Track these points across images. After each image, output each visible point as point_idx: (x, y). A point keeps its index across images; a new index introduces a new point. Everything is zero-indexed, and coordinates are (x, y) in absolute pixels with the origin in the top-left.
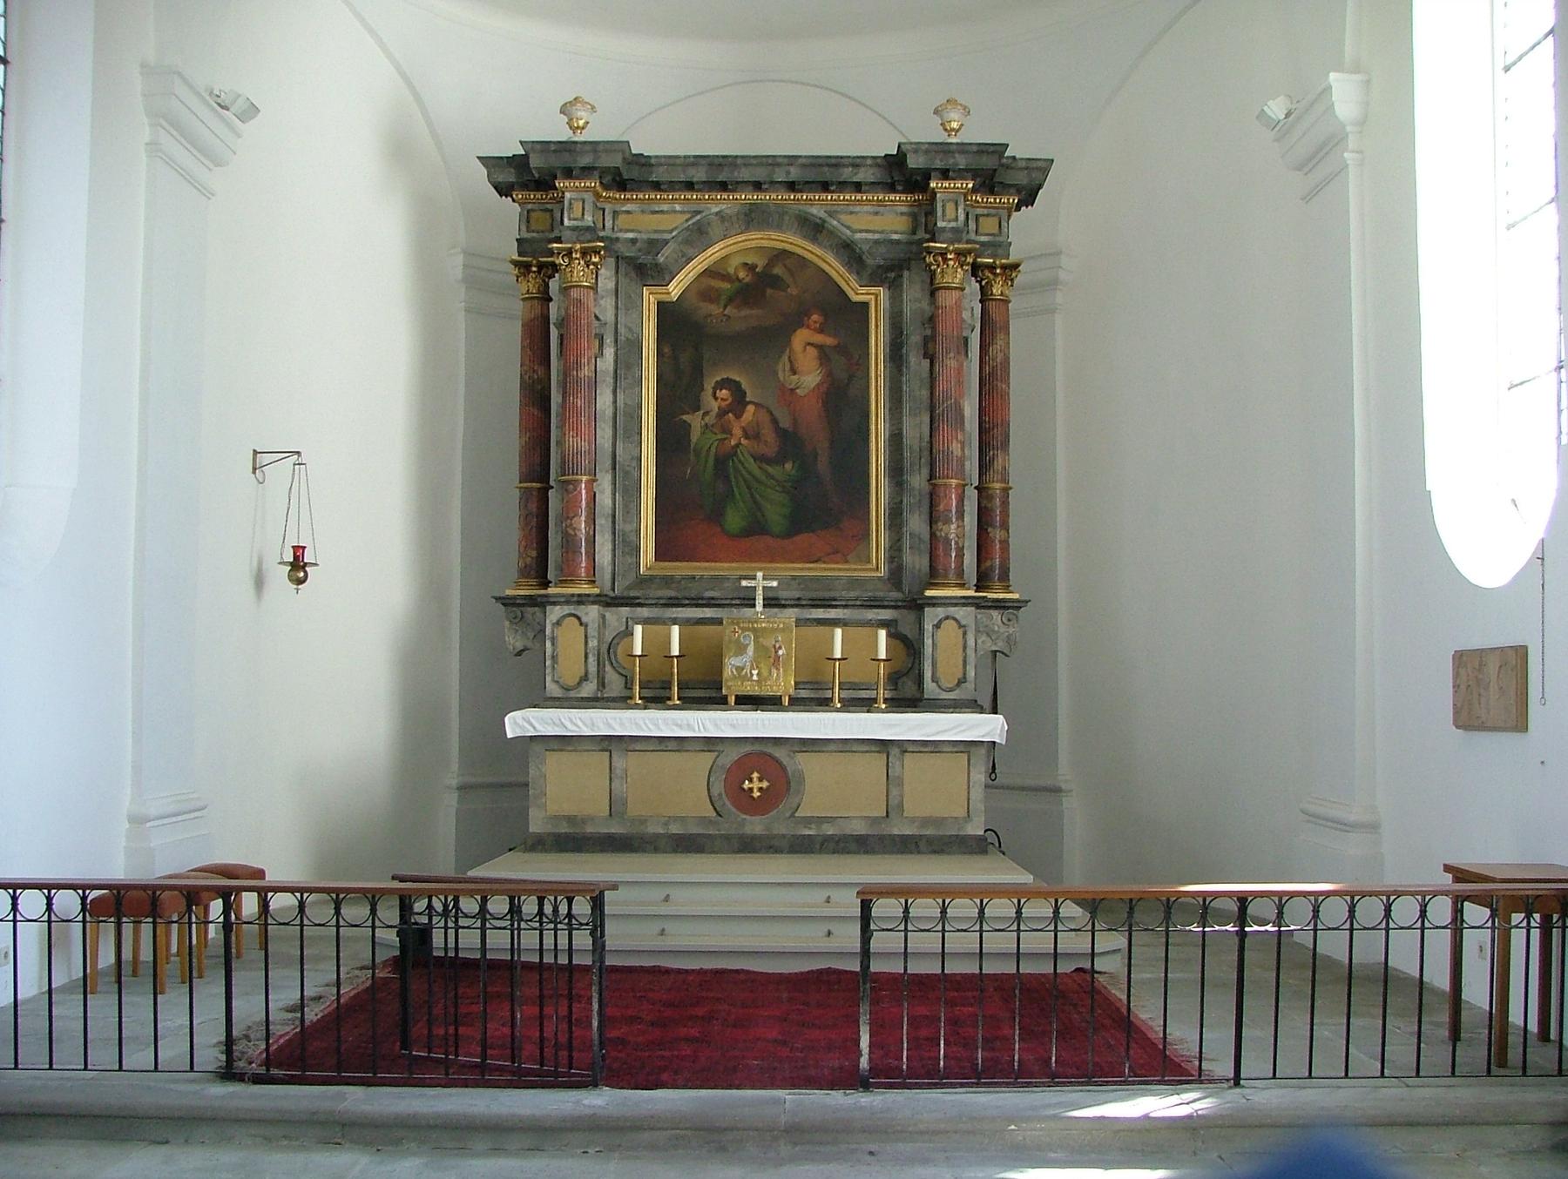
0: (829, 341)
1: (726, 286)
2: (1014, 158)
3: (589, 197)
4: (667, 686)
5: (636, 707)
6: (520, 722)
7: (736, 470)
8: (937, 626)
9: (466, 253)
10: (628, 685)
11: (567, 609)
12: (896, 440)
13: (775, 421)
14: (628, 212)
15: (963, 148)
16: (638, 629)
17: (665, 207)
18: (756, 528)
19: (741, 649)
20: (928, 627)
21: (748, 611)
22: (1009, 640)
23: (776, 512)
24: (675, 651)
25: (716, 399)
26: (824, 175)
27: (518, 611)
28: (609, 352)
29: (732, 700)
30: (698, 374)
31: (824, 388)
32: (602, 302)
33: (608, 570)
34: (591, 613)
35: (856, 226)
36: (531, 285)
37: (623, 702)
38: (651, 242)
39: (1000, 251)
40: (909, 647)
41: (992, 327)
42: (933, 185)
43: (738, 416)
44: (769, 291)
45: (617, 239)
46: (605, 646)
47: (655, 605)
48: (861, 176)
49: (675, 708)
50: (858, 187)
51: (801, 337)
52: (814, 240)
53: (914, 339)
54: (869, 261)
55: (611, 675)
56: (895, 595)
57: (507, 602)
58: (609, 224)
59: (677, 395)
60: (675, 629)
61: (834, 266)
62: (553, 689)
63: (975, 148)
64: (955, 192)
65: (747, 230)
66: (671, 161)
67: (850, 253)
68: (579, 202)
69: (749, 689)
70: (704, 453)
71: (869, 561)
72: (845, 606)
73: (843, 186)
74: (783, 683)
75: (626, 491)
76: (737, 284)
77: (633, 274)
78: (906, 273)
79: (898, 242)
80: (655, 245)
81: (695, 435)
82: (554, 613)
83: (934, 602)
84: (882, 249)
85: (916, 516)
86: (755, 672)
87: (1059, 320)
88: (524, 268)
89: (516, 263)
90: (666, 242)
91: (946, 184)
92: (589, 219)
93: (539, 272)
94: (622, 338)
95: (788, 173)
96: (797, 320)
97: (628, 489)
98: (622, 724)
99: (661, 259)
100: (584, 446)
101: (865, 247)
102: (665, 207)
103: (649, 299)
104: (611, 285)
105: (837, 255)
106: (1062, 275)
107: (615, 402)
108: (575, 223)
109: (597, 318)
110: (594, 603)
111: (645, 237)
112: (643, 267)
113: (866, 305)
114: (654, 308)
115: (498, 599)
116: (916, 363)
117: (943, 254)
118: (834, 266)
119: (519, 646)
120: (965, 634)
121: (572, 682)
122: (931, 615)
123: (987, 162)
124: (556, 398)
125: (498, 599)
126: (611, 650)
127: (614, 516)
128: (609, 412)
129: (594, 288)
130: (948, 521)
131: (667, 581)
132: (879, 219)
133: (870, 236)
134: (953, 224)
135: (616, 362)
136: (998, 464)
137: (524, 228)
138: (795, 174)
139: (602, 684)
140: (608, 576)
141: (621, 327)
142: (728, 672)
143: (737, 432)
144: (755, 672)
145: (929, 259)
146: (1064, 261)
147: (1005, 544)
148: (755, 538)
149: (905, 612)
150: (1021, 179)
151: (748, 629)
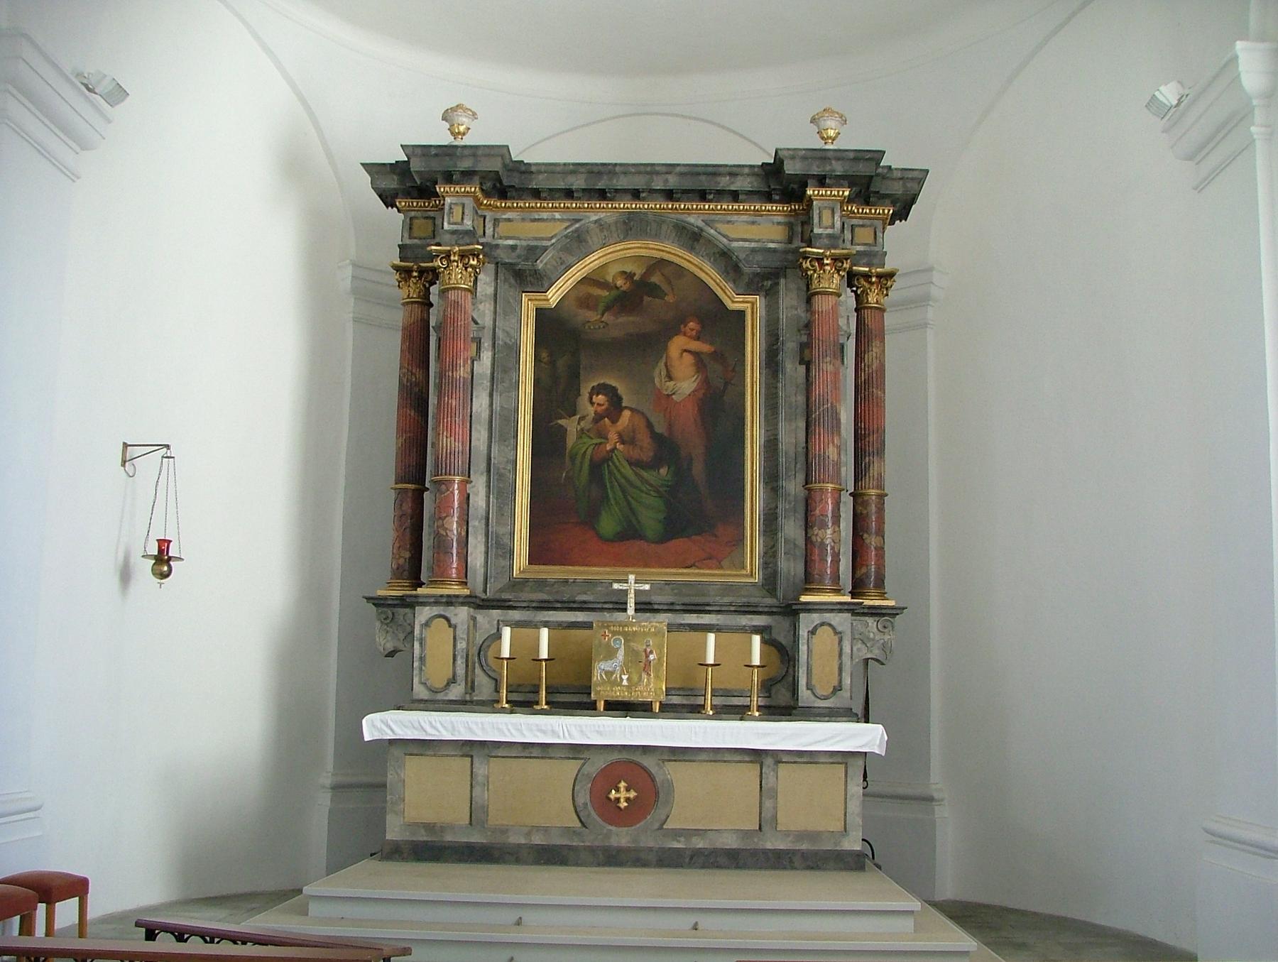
3: (469, 202)
5: (503, 711)
6: (379, 724)
8: (813, 632)
10: (497, 690)
11: (436, 610)
12: (771, 446)
13: (650, 425)
14: (509, 220)
15: (840, 155)
16: (507, 632)
17: (545, 215)
18: (630, 532)
19: (611, 654)
20: (803, 633)
21: (619, 616)
23: (650, 517)
24: (544, 654)
25: (592, 403)
26: (702, 185)
28: (487, 356)
29: (601, 705)
31: (700, 394)
32: (481, 307)
33: (481, 572)
34: (461, 614)
36: (412, 290)
37: (490, 706)
38: (531, 249)
39: (875, 261)
40: (783, 654)
41: (867, 335)
42: (809, 192)
44: (647, 299)
45: (497, 246)
46: (474, 651)
48: (741, 184)
50: (735, 196)
51: (677, 344)
52: (691, 249)
53: (790, 345)
54: (746, 270)
55: (481, 678)
56: (769, 601)
57: (378, 602)
58: (489, 231)
60: (544, 633)
61: (711, 275)
62: (420, 692)
63: (851, 155)
66: (551, 169)
67: (728, 262)
68: (459, 206)
69: (619, 694)
70: (578, 462)
71: (743, 568)
72: (719, 612)
73: (721, 194)
74: (652, 689)
75: (500, 494)
76: (614, 293)
77: (512, 281)
78: (782, 281)
79: (774, 250)
80: (534, 252)
81: (571, 439)
82: (423, 614)
83: (810, 608)
84: (759, 258)
86: (625, 677)
87: (929, 331)
88: (405, 273)
90: (545, 249)
92: (468, 224)
93: (420, 277)
95: (667, 181)
96: (672, 328)
97: (502, 491)
99: (540, 265)
101: (742, 256)
102: (545, 215)
103: (528, 306)
104: (490, 290)
105: (714, 264)
106: (934, 291)
108: (455, 227)
110: (463, 604)
111: (524, 243)
112: (523, 274)
113: (741, 313)
114: (532, 314)
115: (369, 599)
116: (792, 370)
118: (711, 275)
119: (390, 646)
120: (841, 641)
122: (806, 622)
123: (863, 169)
124: (433, 400)
125: (369, 599)
127: (487, 519)
129: (473, 291)
130: (823, 526)
131: (541, 584)
132: (756, 228)
133: (746, 244)
134: (829, 231)
136: (874, 471)
137: (406, 235)
138: (673, 182)
139: (471, 687)
140: (480, 579)
143: (613, 436)
144: (625, 677)
147: (880, 550)
148: (629, 542)
150: (897, 189)
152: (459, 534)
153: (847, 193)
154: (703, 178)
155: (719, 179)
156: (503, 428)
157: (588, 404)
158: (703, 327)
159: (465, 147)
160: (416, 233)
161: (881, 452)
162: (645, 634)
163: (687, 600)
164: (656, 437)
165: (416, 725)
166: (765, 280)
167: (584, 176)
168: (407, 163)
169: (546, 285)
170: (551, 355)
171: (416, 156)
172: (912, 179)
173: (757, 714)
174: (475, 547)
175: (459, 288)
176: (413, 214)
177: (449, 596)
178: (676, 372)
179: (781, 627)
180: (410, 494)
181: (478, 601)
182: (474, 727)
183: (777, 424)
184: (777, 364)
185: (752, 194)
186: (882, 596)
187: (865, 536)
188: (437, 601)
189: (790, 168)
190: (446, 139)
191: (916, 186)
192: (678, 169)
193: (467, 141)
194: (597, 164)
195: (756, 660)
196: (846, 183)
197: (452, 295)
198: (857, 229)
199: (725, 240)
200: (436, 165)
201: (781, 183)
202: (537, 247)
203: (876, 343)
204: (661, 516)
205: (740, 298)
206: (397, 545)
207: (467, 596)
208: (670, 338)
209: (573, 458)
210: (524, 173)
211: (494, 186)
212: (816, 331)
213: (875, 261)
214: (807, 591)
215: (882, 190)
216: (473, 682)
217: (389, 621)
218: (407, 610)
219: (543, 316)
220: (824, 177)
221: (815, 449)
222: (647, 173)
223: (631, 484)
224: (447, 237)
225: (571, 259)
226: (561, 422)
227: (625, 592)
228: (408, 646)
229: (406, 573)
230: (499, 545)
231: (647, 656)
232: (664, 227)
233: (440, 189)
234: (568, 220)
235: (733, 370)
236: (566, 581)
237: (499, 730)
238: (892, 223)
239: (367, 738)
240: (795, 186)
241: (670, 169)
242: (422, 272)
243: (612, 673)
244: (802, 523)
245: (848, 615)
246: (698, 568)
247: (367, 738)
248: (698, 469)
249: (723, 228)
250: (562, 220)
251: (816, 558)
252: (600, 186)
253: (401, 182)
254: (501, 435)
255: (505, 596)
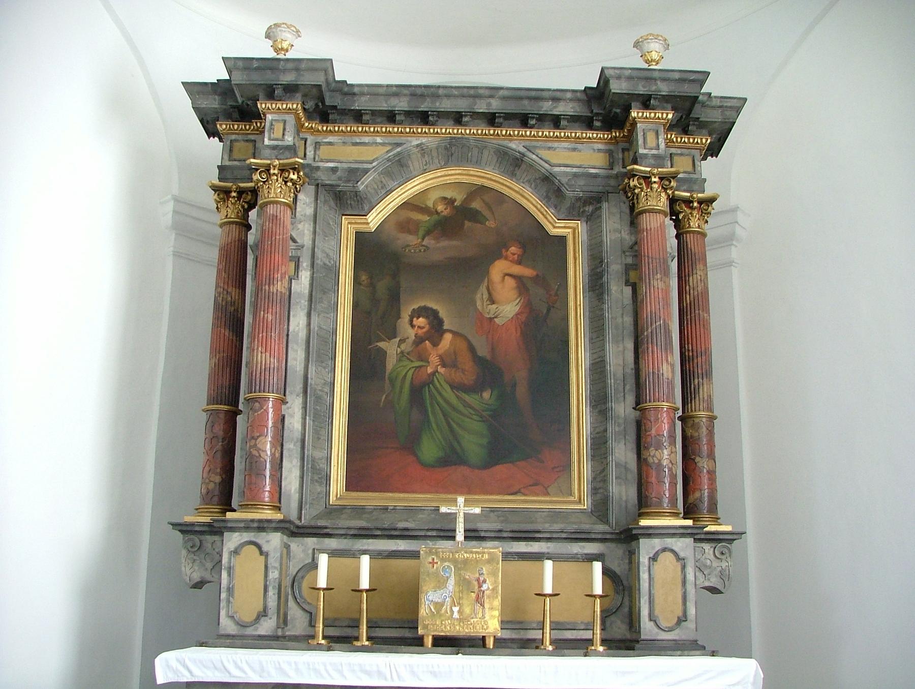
0: (527, 272)
1: (426, 218)
2: (709, 95)
3: (291, 119)
4: (356, 625)
5: (319, 648)
6: (174, 664)
7: (432, 396)
8: (654, 559)
9: (176, 200)
10: (312, 624)
11: (247, 536)
12: (598, 369)
13: (472, 349)
14: (330, 144)
15: (666, 75)
16: (323, 560)
17: (366, 139)
18: (452, 458)
19: (441, 584)
20: (644, 560)
21: (444, 545)
22: (722, 575)
23: (473, 443)
24: (365, 584)
25: (413, 326)
26: (526, 111)
27: (196, 539)
28: (305, 276)
29: (429, 641)
30: (395, 299)
31: (523, 317)
32: (300, 226)
33: (295, 497)
34: (274, 541)
35: (554, 161)
36: (231, 211)
37: (305, 642)
38: (352, 171)
39: (696, 187)
40: (622, 585)
41: (688, 259)
42: (634, 114)
43: (435, 344)
44: (467, 224)
45: (318, 168)
46: (287, 582)
47: (344, 536)
48: (564, 109)
49: (363, 649)
50: (556, 121)
51: (499, 268)
52: (512, 175)
53: (615, 267)
54: (569, 194)
55: (295, 612)
56: (601, 527)
57: (185, 529)
58: (310, 153)
59: (373, 322)
60: (365, 560)
61: (531, 201)
62: (227, 625)
63: (677, 76)
64: (655, 120)
65: (446, 165)
66: (373, 90)
67: (550, 187)
68: (280, 122)
69: (448, 629)
70: (398, 384)
71: (571, 494)
72: (549, 539)
73: (542, 119)
74: (491, 623)
75: (316, 416)
76: (435, 217)
77: (332, 203)
78: (605, 205)
79: (595, 176)
80: (355, 174)
81: (391, 363)
82: (233, 540)
83: (650, 533)
84: (581, 182)
85: (622, 445)
86: (456, 609)
87: (735, 271)
88: (223, 193)
89: (215, 189)
90: (366, 171)
91: (647, 114)
92: (289, 139)
93: (239, 198)
94: (318, 262)
95: (489, 104)
96: (495, 253)
97: (319, 414)
98: (297, 670)
99: (361, 187)
100: (274, 363)
101: (564, 180)
102: (366, 139)
103: (348, 227)
104: (310, 211)
105: (536, 189)
106: (738, 230)
107: (309, 324)
108: (276, 143)
109: (294, 241)
110: (276, 530)
111: (345, 166)
112: (344, 197)
113: (562, 239)
114: (352, 238)
115: (175, 525)
116: (618, 292)
117: (647, 179)
118: (531, 201)
119: (196, 577)
120: (684, 567)
121: (248, 617)
122: (646, 548)
123: (687, 90)
124: (248, 319)
125: (175, 525)
126: (295, 585)
127: (303, 441)
128: (303, 335)
129: (293, 206)
130: (659, 446)
131: (359, 511)
132: (578, 155)
133: (568, 170)
134: (654, 152)
135: (311, 285)
136: (703, 393)
137: (226, 157)
138: (495, 105)
139: (284, 620)
140: (294, 505)
141: (316, 250)
142: (423, 611)
143: (434, 359)
144: (456, 609)
145: (634, 183)
146: (740, 217)
147: (712, 473)
148: (451, 469)
149: (612, 545)
150: (715, 116)
151: (449, 560)
152: (273, 455)
153: (670, 116)
154: (526, 102)
155: (541, 104)
156: (320, 349)
157: (408, 326)
158: (525, 252)
159: (288, 60)
160: (236, 155)
161: (708, 374)
162: (477, 561)
163: (516, 527)
164: (479, 360)
165: (219, 665)
166: (587, 206)
167: (406, 99)
168: (229, 81)
169: (366, 208)
170: (371, 278)
171: (237, 69)
172: (731, 107)
173: (601, 649)
174: (290, 471)
175: (277, 202)
176: (233, 137)
177: (260, 521)
178: (497, 296)
179: (616, 552)
180: (222, 416)
181: (292, 528)
182: (285, 667)
183: (604, 345)
184: (602, 285)
185: (575, 120)
186: (716, 520)
187: (698, 459)
188: (248, 526)
189: (616, 87)
190: (271, 54)
191: (734, 114)
192: (501, 93)
193: (289, 55)
194: (420, 86)
195: (598, 589)
196: (669, 106)
197: (271, 210)
198: (675, 158)
199: (546, 166)
200: (257, 78)
201: (606, 109)
202: (358, 169)
203: (700, 266)
204: (485, 441)
205: (562, 223)
206: (207, 469)
207: (281, 521)
208: (495, 260)
209: (392, 382)
210: (346, 94)
211: (317, 105)
212: (645, 250)
213: (696, 187)
214: (641, 515)
215: (701, 118)
216: (286, 615)
217: (196, 550)
218: (216, 538)
219: (361, 237)
220: (649, 97)
221: (647, 367)
222: (470, 96)
223: (454, 408)
224: (267, 152)
225: (392, 184)
226: (381, 344)
227: (452, 517)
228: (217, 577)
229: (216, 499)
230: (315, 469)
231: (480, 586)
232: (486, 153)
233: (261, 106)
234: (390, 144)
235: (556, 295)
236: (385, 509)
237: (317, 671)
238: (704, 159)
239: (160, 680)
240: (618, 111)
241: (492, 92)
242: (241, 192)
243: (442, 604)
244: (634, 446)
245: (690, 541)
246: (525, 495)
247: (160, 680)
248: (522, 391)
249: (545, 154)
250: (383, 144)
251: (653, 479)
252: (423, 108)
253: (223, 103)
254: (318, 356)
255: (321, 523)
